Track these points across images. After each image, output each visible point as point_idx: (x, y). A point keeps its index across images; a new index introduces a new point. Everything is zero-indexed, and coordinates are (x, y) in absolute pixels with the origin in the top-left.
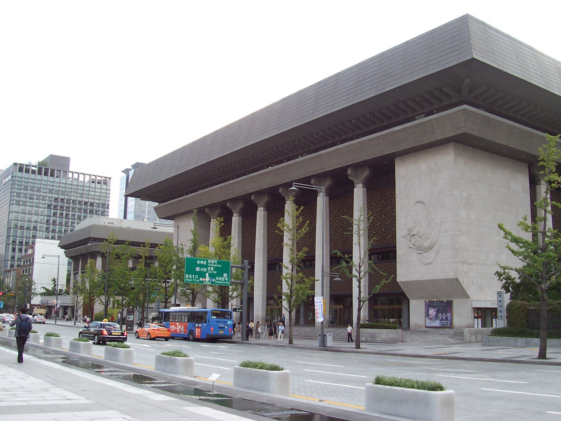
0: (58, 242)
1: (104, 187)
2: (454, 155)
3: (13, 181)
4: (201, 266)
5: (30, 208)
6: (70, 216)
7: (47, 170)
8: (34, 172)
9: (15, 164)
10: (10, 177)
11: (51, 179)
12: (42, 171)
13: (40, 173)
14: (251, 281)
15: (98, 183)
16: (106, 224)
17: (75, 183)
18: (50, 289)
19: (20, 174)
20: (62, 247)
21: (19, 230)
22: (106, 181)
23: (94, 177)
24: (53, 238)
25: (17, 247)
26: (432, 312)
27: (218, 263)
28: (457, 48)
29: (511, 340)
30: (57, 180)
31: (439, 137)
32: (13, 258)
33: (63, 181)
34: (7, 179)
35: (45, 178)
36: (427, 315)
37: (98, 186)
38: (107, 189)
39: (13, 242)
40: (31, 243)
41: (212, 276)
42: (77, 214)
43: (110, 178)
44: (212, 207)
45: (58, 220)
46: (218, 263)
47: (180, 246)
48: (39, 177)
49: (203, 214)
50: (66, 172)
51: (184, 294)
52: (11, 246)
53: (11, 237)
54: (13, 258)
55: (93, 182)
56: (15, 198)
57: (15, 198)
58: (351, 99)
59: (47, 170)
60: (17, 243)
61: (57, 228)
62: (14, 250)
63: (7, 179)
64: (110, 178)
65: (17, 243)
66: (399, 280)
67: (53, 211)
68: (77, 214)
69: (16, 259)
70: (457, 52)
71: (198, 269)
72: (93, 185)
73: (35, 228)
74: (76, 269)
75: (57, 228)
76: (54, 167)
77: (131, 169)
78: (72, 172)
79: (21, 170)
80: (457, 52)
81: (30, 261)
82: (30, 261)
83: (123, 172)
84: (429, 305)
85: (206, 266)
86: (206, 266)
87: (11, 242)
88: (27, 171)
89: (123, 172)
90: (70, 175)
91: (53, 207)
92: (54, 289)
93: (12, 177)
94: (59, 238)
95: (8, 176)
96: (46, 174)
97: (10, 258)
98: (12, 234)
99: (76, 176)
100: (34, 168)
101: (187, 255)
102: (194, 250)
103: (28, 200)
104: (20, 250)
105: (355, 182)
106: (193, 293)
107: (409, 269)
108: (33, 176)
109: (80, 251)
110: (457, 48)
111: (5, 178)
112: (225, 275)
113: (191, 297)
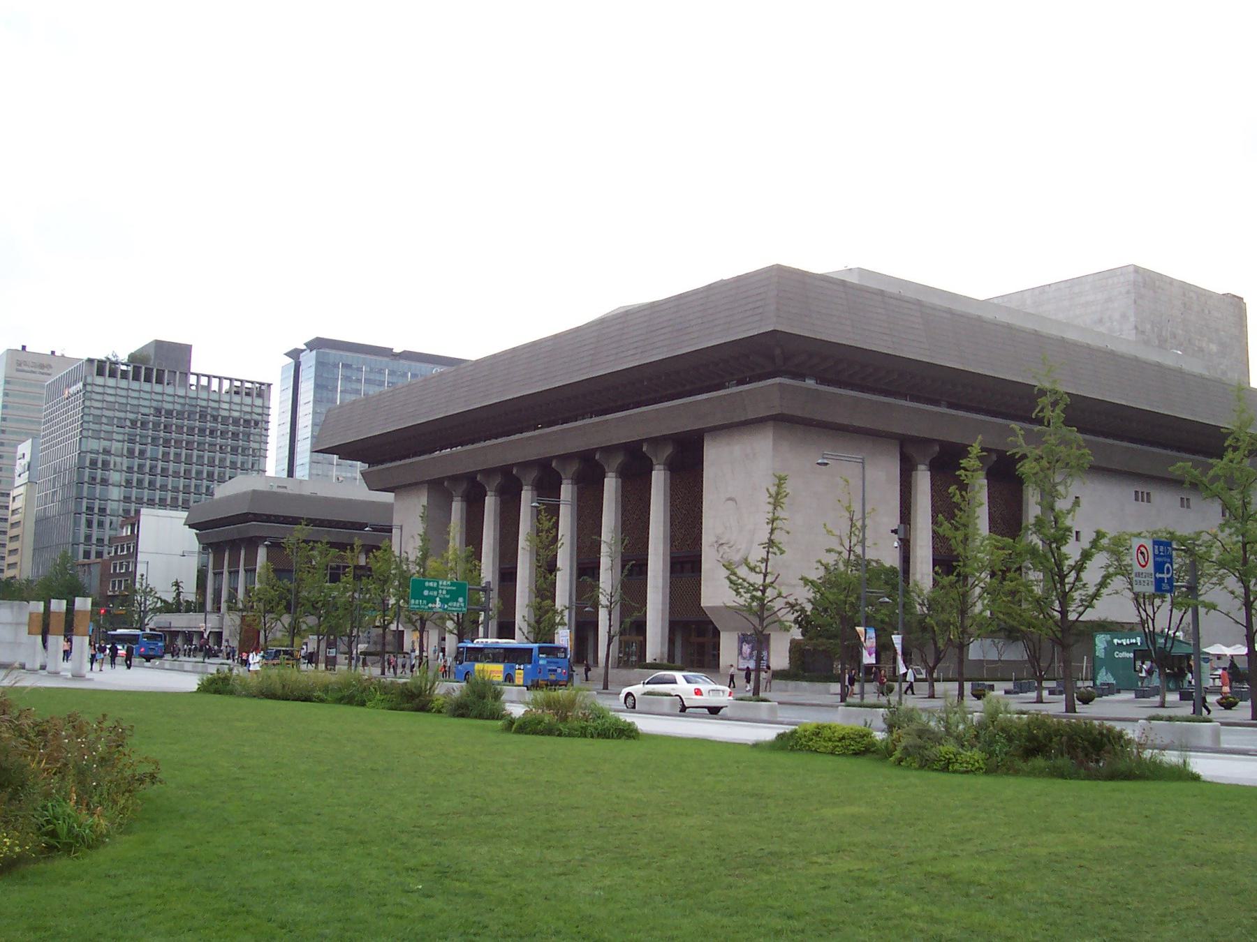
0: (185, 514)
1: (258, 402)
2: (774, 440)
3: (86, 394)
4: (430, 589)
5: (120, 444)
6: (194, 460)
7: (149, 372)
8: (124, 375)
9: (90, 361)
10: (80, 385)
11: (158, 388)
12: (139, 373)
13: (136, 377)
14: (551, 577)
15: (247, 394)
16: (275, 489)
17: (204, 395)
18: (170, 600)
19: (99, 380)
20: (191, 526)
21: (98, 487)
22: (261, 391)
23: (238, 384)
24: (174, 506)
25: (96, 519)
26: (746, 648)
27: (452, 584)
28: (761, 310)
29: (791, 684)
30: (169, 390)
31: (751, 416)
32: (88, 538)
33: (181, 392)
34: (74, 389)
35: (147, 387)
36: (740, 652)
37: (248, 400)
38: (263, 407)
39: (88, 508)
40: (132, 513)
41: (443, 601)
42: (207, 454)
43: (269, 385)
44: (455, 479)
45: (171, 466)
46: (452, 584)
47: (404, 555)
48: (135, 385)
49: (440, 489)
50: (186, 374)
51: (410, 621)
52: (84, 517)
53: (85, 501)
54: (88, 538)
55: (236, 393)
56: (92, 426)
57: (92, 426)
58: (637, 357)
59: (149, 372)
60: (96, 510)
61: (170, 482)
62: (89, 524)
63: (74, 389)
64: (269, 385)
65: (96, 510)
66: (705, 603)
67: (161, 449)
68: (207, 454)
69: (94, 540)
70: (757, 318)
71: (426, 593)
72: (237, 399)
73: (105, 464)
74: (218, 564)
75: (170, 482)
76: (162, 363)
77: (303, 351)
78: (197, 375)
79: (100, 372)
80: (757, 318)
81: (129, 548)
82: (129, 548)
83: (288, 354)
84: (743, 639)
85: (437, 589)
86: (437, 589)
87: (84, 509)
88: (113, 374)
89: (288, 354)
90: (193, 380)
91: (161, 441)
92: (178, 603)
93: (84, 385)
94: (185, 506)
95: (75, 383)
96: (148, 380)
97: (82, 540)
98: (85, 494)
99: (204, 381)
100: (124, 368)
101: (414, 569)
102: (422, 561)
103: (115, 429)
104: (101, 524)
105: (654, 461)
106: (421, 619)
107: (715, 592)
108: (124, 383)
109: (225, 537)
110: (761, 310)
111: (69, 386)
112: (461, 599)
113: (418, 624)
